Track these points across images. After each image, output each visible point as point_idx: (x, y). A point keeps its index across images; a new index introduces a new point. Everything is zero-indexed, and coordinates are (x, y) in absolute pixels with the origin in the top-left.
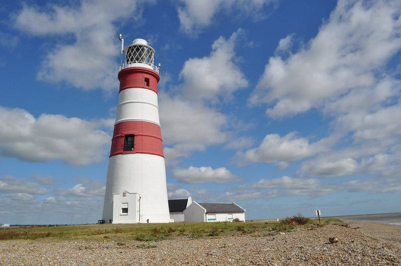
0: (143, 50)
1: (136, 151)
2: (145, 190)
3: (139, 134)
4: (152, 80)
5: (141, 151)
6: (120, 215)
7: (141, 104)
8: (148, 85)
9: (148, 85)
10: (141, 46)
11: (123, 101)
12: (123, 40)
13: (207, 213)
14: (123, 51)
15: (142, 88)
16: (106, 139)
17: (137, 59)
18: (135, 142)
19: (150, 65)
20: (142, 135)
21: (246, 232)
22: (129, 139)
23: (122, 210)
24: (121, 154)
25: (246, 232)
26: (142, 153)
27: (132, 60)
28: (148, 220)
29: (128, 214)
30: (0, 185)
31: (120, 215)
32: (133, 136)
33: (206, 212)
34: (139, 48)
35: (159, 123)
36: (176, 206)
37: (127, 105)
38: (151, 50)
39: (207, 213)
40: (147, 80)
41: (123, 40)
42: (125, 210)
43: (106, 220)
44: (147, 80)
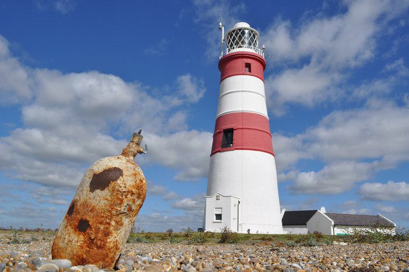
0: (243, 33)
1: (236, 147)
2: (250, 193)
3: (238, 127)
4: (255, 65)
5: (241, 147)
6: (213, 222)
7: (241, 93)
8: (250, 71)
9: (250, 71)
10: (240, 30)
11: (222, 92)
12: (223, 28)
13: (335, 226)
14: (224, 40)
15: (242, 74)
16: (207, 140)
17: (237, 43)
18: (234, 137)
19: (251, 48)
20: (242, 128)
21: (285, 62)
22: (229, 135)
23: (215, 217)
24: (219, 151)
25: (285, 62)
26: (242, 149)
27: (232, 45)
28: (249, 230)
29: (222, 221)
30: (403, 188)
31: (213, 222)
32: (231, 131)
33: (333, 223)
34: (242, 31)
35: (267, 115)
36: (290, 219)
37: (227, 96)
38: (252, 31)
39: (335, 226)
40: (248, 66)
41: (223, 28)
42: (219, 217)
43: (201, 230)
44: (248, 66)
